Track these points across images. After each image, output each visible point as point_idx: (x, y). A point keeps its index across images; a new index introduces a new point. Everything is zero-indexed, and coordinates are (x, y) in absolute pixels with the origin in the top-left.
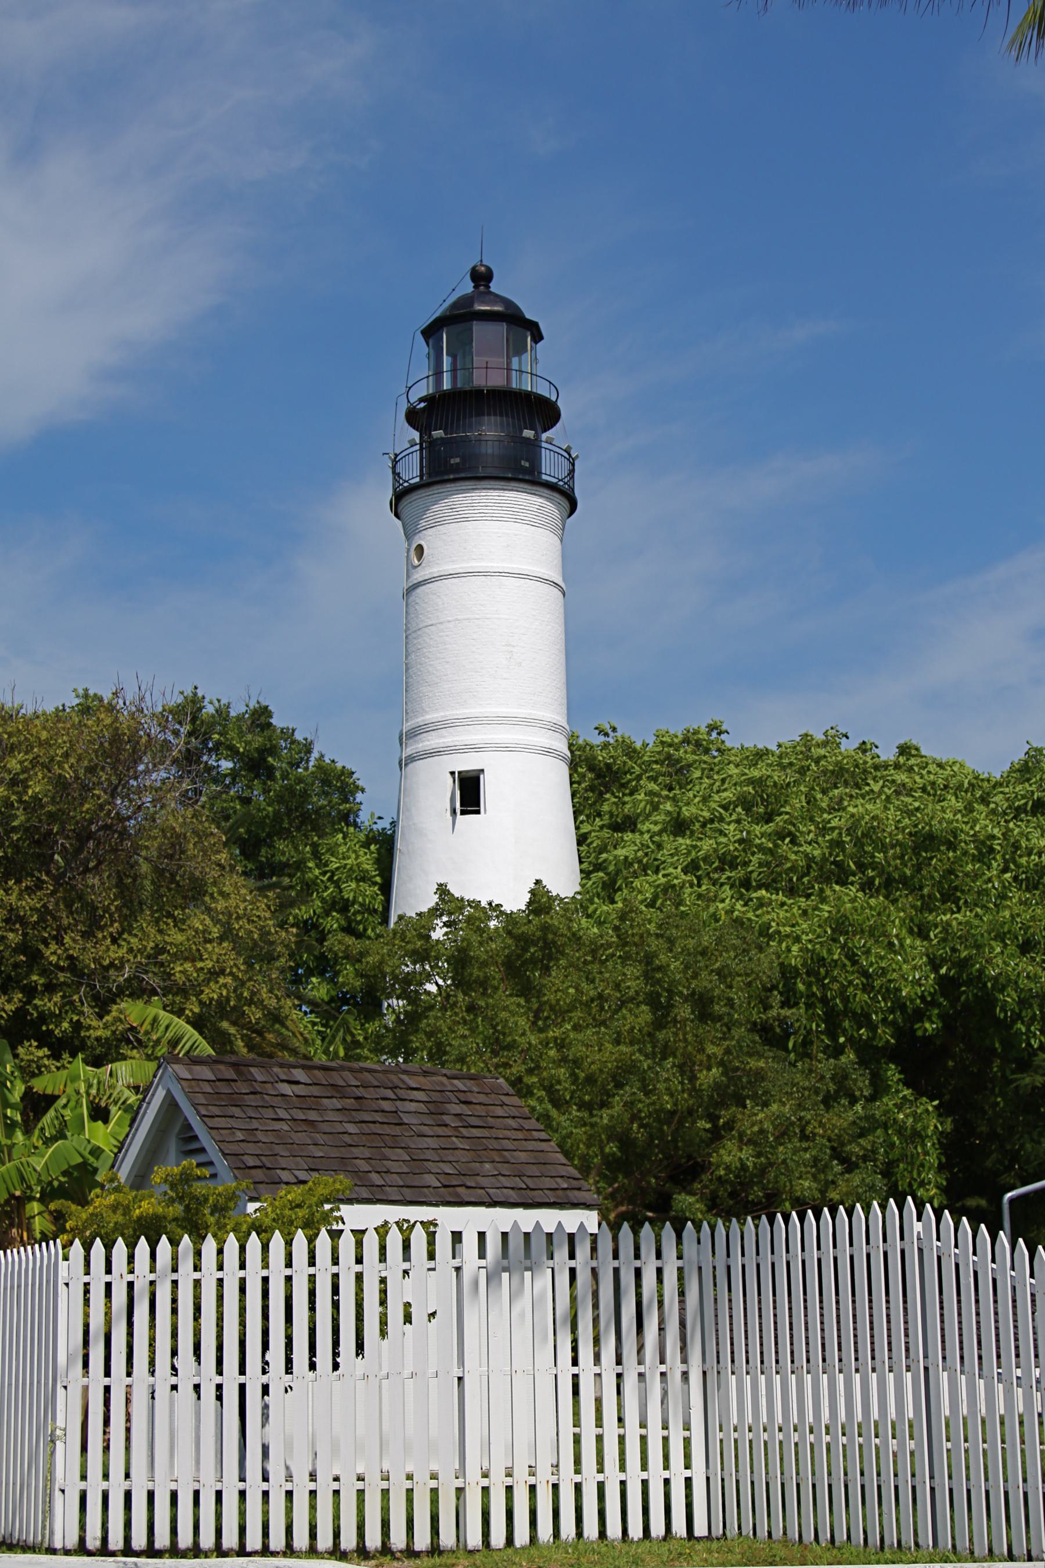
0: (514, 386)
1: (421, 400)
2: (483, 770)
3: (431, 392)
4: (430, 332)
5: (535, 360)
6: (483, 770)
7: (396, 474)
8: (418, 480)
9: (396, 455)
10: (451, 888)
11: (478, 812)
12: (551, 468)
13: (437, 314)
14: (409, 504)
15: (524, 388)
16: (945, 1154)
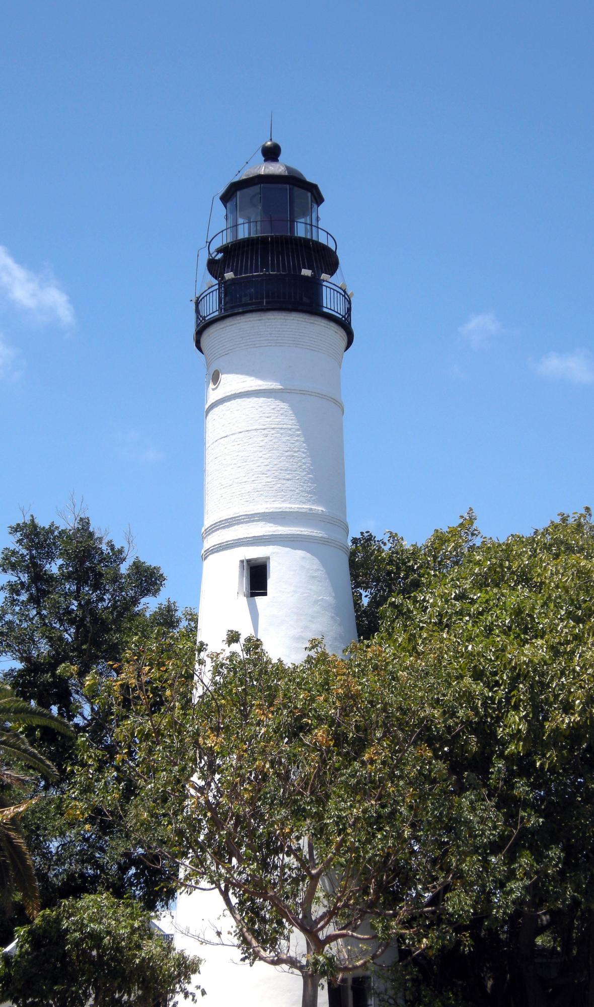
1: (219, 251)
3: (225, 243)
4: (226, 198)
7: (197, 311)
8: (217, 313)
11: (265, 594)
12: (331, 302)
14: (212, 336)
16: (538, 950)
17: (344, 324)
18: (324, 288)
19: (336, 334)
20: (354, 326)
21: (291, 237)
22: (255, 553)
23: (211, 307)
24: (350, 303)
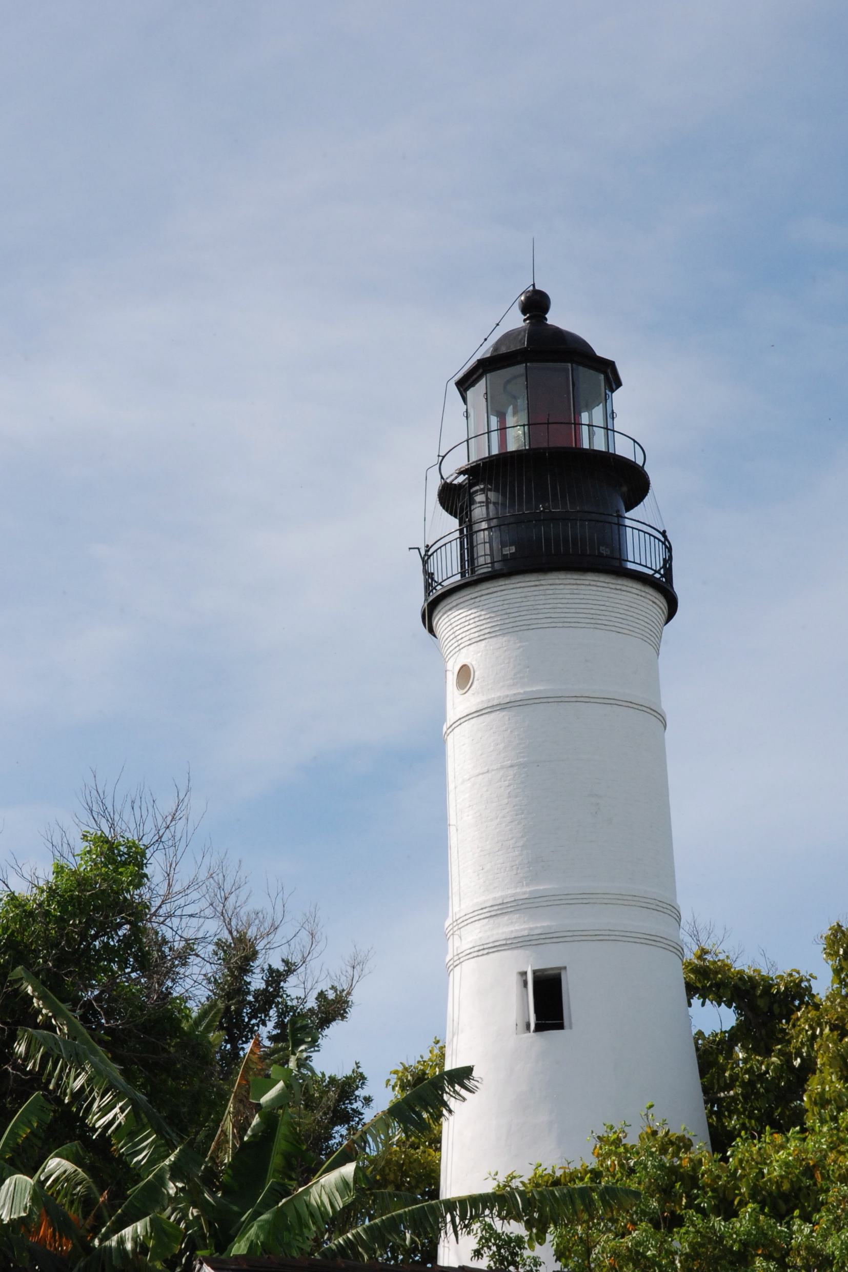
0: (586, 445)
2: (565, 968)
3: (473, 458)
5: (610, 415)
6: (565, 968)
9: (428, 548)
10: (335, 1030)
11: (560, 1026)
12: (640, 553)
13: (478, 356)
15: (596, 448)
17: (662, 586)
18: (629, 530)
19: (649, 603)
20: (679, 586)
21: (576, 448)
22: (548, 961)
23: (448, 568)
24: (670, 549)
